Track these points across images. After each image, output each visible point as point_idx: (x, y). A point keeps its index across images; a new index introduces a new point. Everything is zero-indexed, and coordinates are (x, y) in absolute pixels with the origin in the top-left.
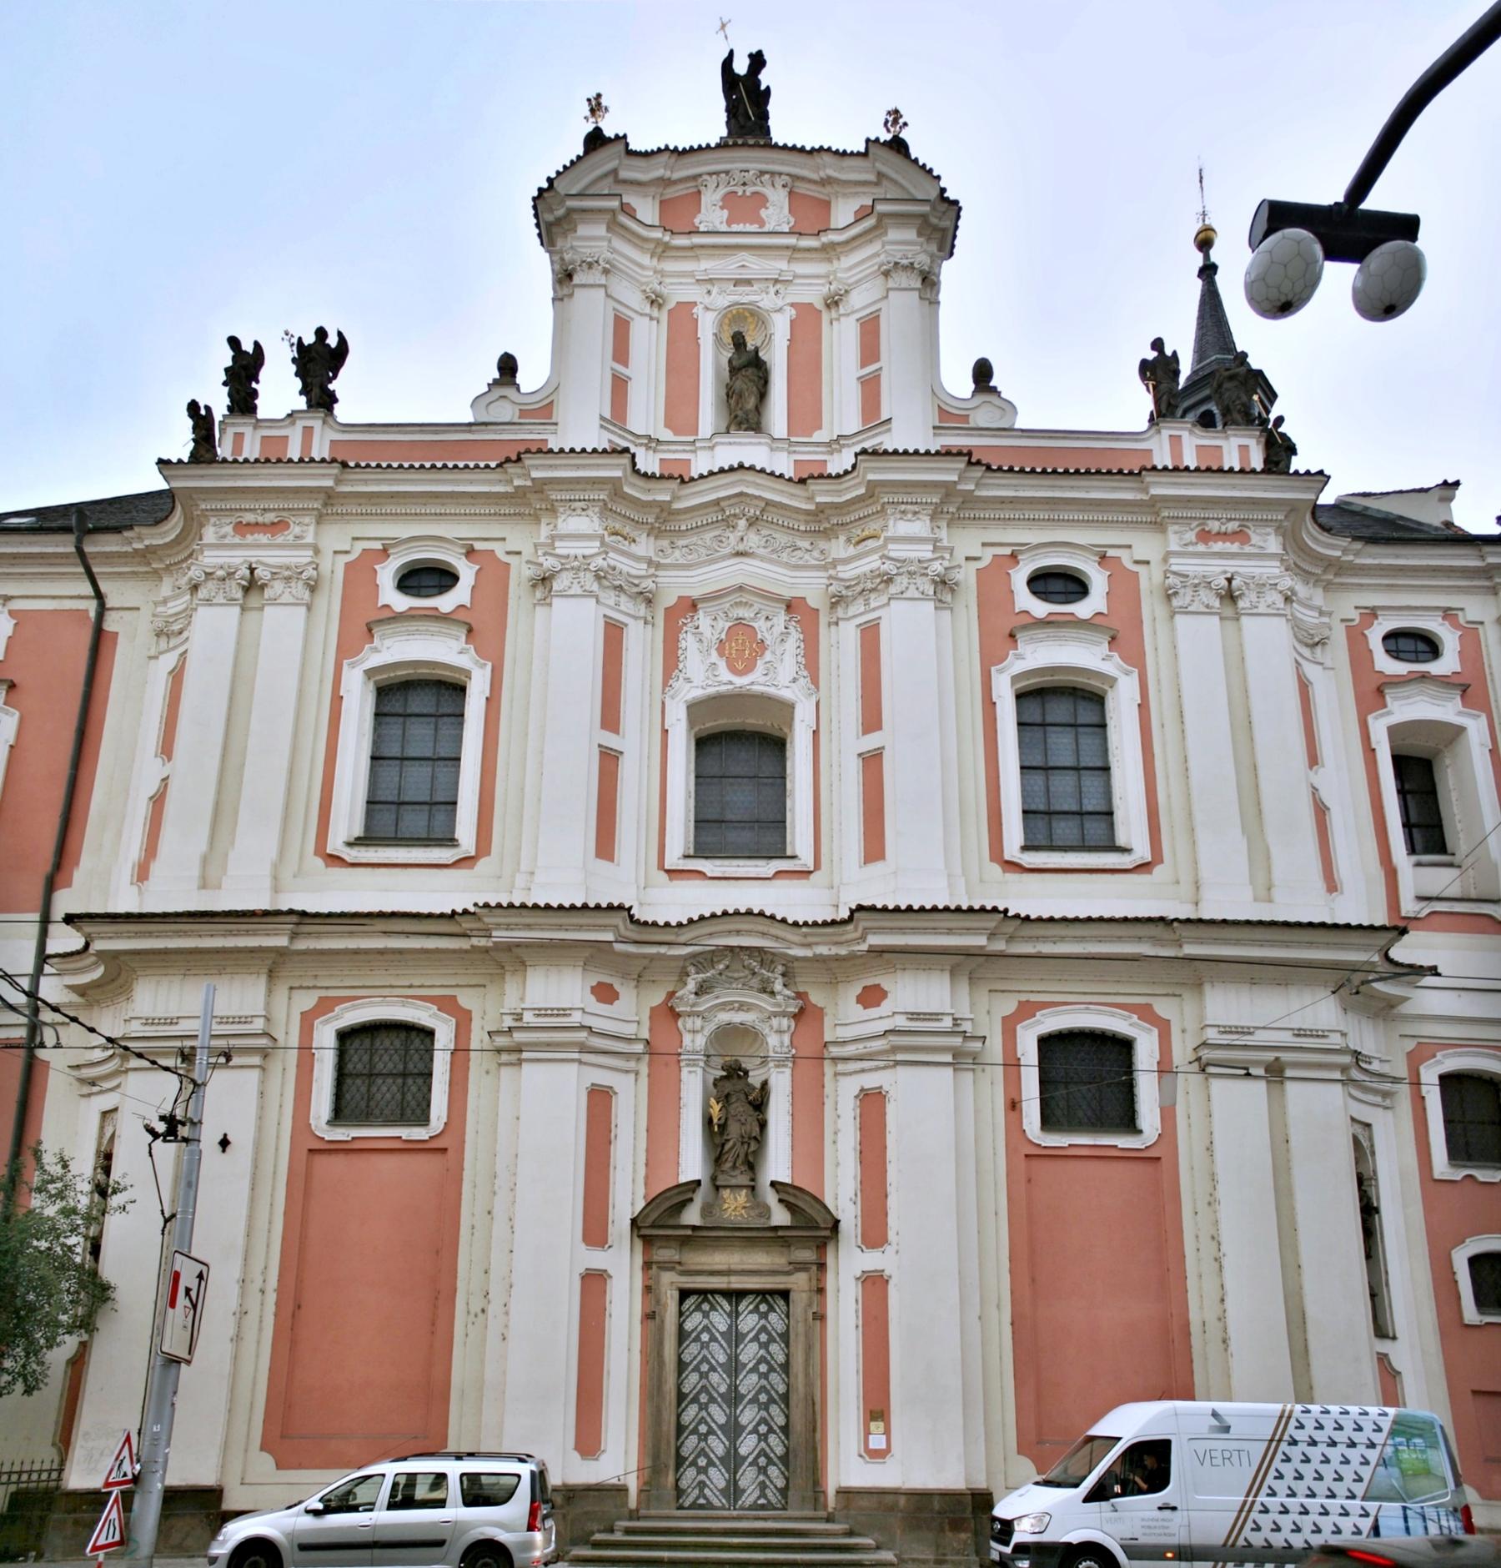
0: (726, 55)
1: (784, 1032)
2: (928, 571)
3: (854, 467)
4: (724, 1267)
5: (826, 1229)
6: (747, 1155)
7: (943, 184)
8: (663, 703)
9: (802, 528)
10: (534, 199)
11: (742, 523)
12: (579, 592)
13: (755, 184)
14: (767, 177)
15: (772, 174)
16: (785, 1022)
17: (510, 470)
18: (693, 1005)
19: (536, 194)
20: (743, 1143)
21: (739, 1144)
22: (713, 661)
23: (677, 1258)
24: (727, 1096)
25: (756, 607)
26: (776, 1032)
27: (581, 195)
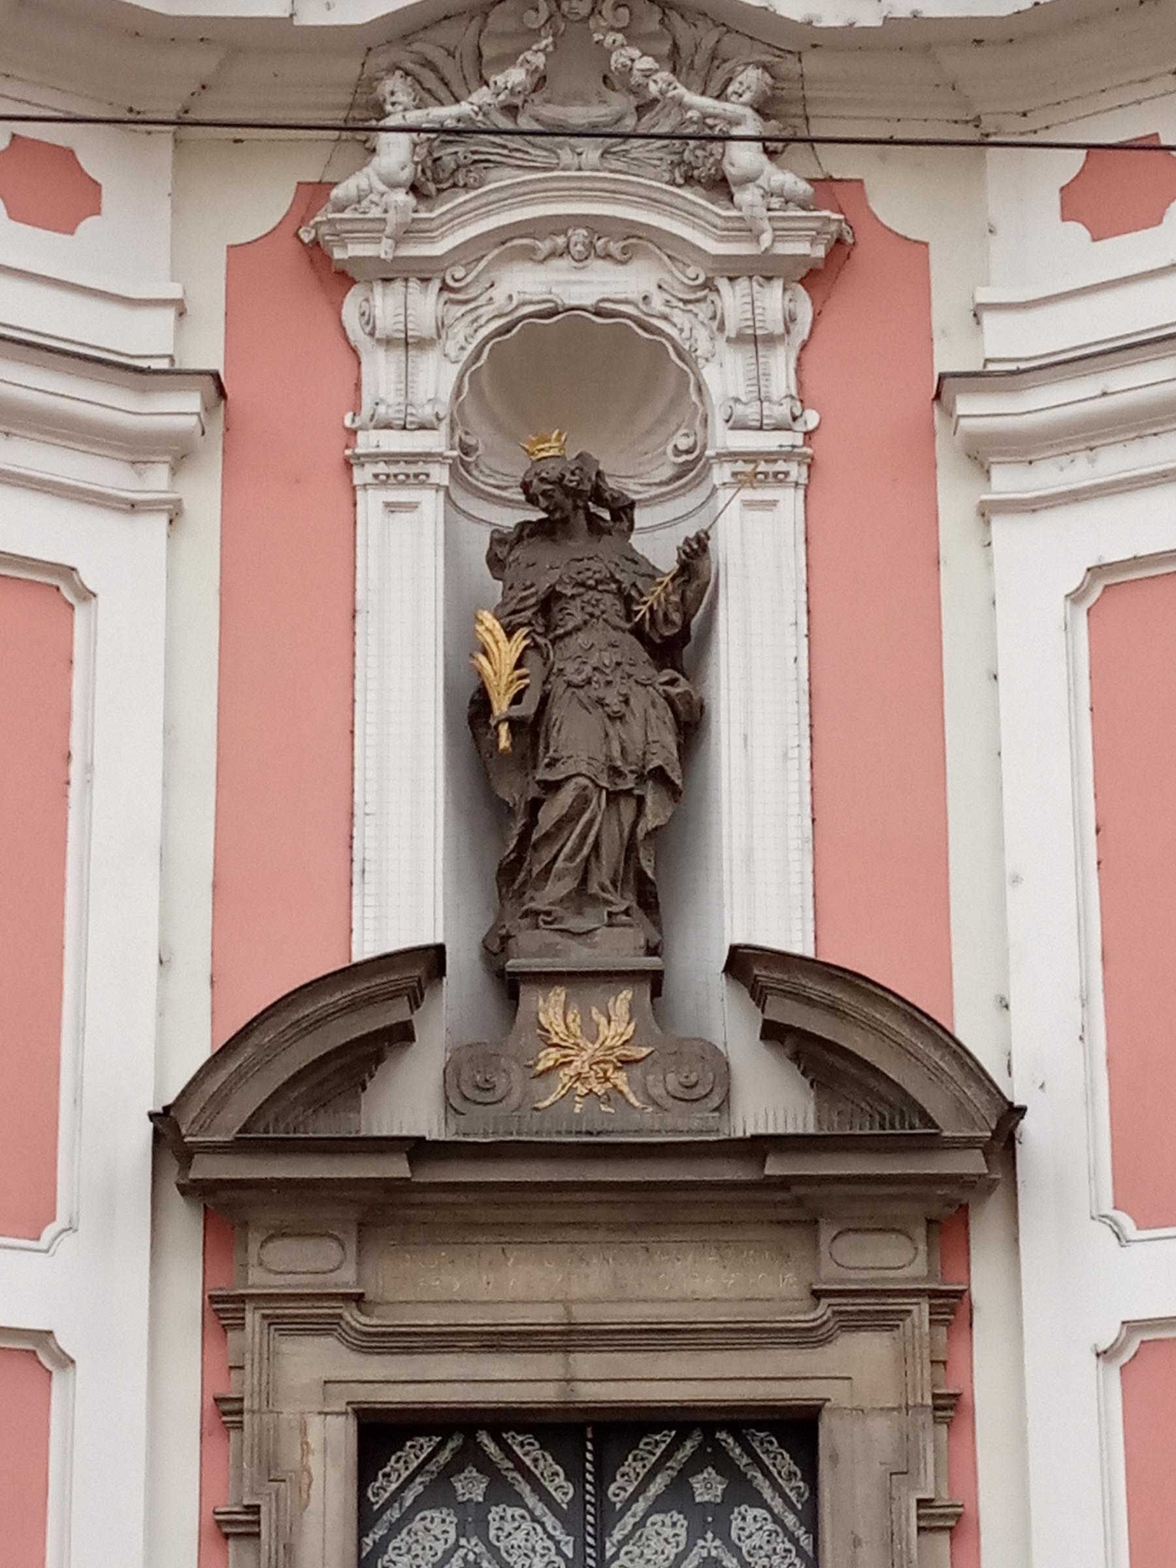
1: (771, 340)
5: (968, 1144)
6: (630, 849)
18: (408, 232)
20: (614, 797)
24: (549, 603)
26: (739, 339)
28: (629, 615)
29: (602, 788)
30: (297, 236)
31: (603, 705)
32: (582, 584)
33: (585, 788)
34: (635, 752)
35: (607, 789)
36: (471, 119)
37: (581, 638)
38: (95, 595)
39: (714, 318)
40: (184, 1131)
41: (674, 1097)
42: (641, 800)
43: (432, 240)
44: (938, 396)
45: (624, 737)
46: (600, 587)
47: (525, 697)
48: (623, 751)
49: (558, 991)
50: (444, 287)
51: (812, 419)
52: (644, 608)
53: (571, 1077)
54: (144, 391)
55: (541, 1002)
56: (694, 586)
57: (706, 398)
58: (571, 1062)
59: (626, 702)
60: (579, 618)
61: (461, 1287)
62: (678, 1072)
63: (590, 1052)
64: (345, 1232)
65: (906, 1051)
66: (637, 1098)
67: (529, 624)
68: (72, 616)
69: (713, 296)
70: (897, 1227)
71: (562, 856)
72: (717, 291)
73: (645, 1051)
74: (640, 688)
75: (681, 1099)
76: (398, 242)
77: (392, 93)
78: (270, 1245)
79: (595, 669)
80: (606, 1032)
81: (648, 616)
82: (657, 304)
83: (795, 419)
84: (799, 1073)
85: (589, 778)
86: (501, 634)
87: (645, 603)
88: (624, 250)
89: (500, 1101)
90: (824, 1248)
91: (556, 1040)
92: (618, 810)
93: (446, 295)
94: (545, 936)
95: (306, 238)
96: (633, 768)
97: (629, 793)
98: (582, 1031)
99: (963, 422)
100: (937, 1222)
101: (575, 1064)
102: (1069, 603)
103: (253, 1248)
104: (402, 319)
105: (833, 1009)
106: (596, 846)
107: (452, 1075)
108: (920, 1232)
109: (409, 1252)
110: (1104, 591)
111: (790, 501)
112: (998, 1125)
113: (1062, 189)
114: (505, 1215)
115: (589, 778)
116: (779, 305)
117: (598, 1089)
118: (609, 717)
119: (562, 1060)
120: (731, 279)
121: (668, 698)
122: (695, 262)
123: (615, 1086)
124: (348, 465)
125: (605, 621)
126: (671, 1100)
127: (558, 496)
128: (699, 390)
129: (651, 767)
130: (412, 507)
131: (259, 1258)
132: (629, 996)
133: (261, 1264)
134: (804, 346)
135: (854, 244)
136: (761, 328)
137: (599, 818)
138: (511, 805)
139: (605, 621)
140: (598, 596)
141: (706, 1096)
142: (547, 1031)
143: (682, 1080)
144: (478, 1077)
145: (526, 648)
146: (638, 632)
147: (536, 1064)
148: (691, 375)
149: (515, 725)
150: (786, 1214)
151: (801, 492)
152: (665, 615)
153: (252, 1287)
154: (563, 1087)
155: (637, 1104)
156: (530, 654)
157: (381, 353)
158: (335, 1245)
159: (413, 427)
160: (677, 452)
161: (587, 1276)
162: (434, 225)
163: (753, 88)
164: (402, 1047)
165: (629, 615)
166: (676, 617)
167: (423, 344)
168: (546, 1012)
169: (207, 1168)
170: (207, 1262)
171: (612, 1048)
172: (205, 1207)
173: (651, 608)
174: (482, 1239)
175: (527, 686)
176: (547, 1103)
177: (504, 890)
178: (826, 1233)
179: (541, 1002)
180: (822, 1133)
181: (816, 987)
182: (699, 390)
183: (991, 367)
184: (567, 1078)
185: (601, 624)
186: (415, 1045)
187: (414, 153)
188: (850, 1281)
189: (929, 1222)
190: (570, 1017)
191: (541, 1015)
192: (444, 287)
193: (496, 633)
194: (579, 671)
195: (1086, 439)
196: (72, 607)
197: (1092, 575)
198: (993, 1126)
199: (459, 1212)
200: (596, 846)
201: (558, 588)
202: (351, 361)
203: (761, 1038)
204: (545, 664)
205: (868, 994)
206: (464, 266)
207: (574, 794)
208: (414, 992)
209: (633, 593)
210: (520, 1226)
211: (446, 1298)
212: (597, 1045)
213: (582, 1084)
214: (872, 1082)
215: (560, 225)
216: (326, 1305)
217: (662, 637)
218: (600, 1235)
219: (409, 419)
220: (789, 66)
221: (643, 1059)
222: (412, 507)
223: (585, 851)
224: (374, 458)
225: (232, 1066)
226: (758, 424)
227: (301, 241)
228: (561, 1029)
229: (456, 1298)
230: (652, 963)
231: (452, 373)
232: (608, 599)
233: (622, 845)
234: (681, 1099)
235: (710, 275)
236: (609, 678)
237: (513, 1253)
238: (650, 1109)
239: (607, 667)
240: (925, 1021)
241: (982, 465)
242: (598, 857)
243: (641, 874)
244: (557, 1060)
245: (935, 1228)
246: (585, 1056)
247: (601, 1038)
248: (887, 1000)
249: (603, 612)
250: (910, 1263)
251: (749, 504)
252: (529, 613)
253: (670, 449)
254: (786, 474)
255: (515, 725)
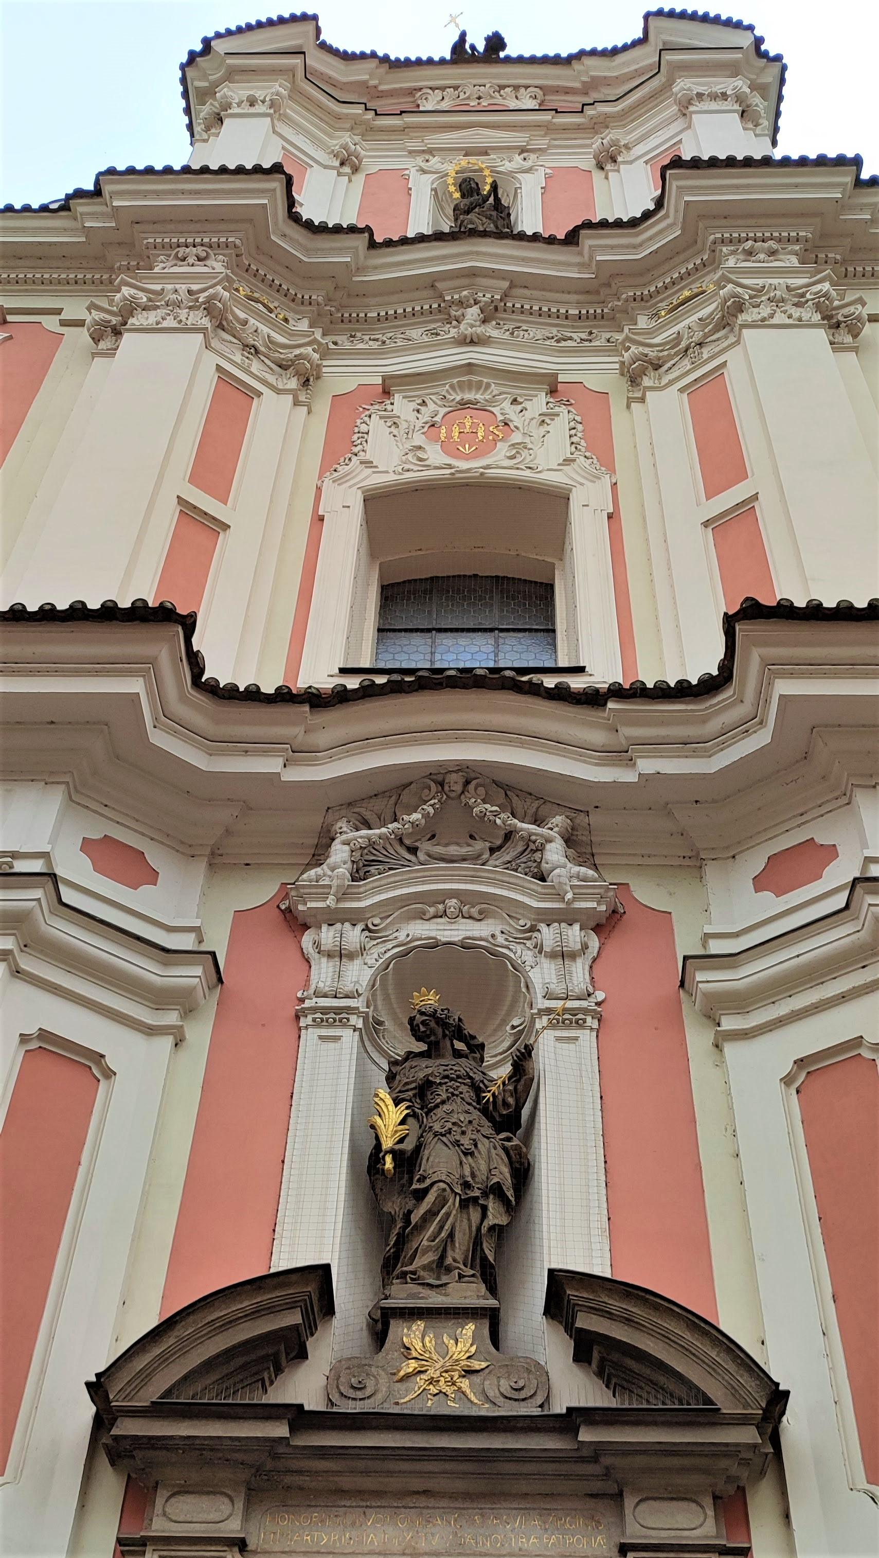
0: (456, 38)
1: (573, 956)
2: (808, 296)
3: (660, 203)
4: (478, 936)
5: (742, 1421)
6: (477, 1242)
7: (758, 33)
8: (319, 489)
9: (573, 312)
10: (183, 67)
11: (473, 313)
12: (175, 324)
13: (492, 97)
14: (508, 90)
15: (516, 88)
16: (574, 935)
17: (80, 209)
18: (344, 895)
19: (184, 58)
20: (465, 1204)
21: (453, 1204)
22: (417, 443)
23: (233, 1527)
24: (425, 1088)
25: (494, 389)
26: (553, 955)
27: (158, 1410)
28: (479, 1099)
29: (456, 1194)
30: (278, 906)
31: (458, 1146)
32: (447, 1077)
33: (444, 1190)
34: (482, 1176)
35: (460, 1195)
36: (387, 837)
37: (446, 1107)
38: (115, 1074)
39: (535, 947)
40: (111, 1397)
41: (506, 1397)
42: (484, 1209)
43: (359, 899)
44: (682, 984)
45: (473, 1165)
46: (460, 1080)
47: (406, 1141)
48: (473, 1175)
49: (419, 1323)
50: (367, 928)
51: (600, 996)
52: (489, 1095)
53: (426, 1381)
54: (166, 964)
55: (405, 1330)
56: (522, 1082)
57: (532, 990)
58: (426, 1371)
59: (476, 1146)
60: (444, 1096)
61: (329, 1540)
62: (508, 1378)
63: (441, 1364)
64: (235, 1491)
65: (686, 1351)
66: (476, 1397)
67: (410, 1101)
68: (98, 1085)
69: (535, 934)
70: (688, 1496)
71: (425, 1238)
72: (539, 930)
73: (484, 1365)
74: (485, 1139)
75: (510, 1399)
76: (338, 900)
77: (341, 828)
78: (173, 1500)
79: (454, 1124)
80: (454, 1349)
81: (491, 1099)
82: (501, 939)
83: (589, 995)
84: (604, 1386)
85: (448, 1184)
86: (390, 1102)
87: (489, 1091)
88: (480, 913)
89: (369, 1397)
90: (628, 1511)
91: (414, 1354)
92: (468, 1214)
93: (366, 933)
94: (412, 1288)
95: (283, 907)
96: (479, 1186)
97: (475, 1199)
98: (435, 1349)
99: (700, 985)
100: (721, 1498)
101: (428, 1372)
102: (783, 1085)
103: (159, 1501)
104: (339, 939)
105: (628, 1321)
106: (451, 1235)
107: (334, 1377)
108: (708, 1502)
109: (287, 1512)
110: (806, 1076)
111: (587, 1038)
112: (768, 1404)
113: (753, 879)
114: (369, 1483)
115: (448, 1184)
116: (578, 939)
117: (449, 1390)
118: (463, 1152)
119: (419, 1369)
120: (548, 925)
121: (505, 1149)
122: (523, 915)
123: (460, 1388)
124: (297, 1018)
125: (462, 1098)
126: (502, 1399)
127: (433, 1024)
128: (527, 987)
129: (492, 1183)
130: (337, 1039)
131: (163, 1510)
132: (473, 1327)
133: (164, 1514)
134: (594, 960)
135: (625, 912)
136: (565, 946)
137: (454, 1212)
138: (393, 1213)
139: (462, 1098)
140: (459, 1084)
141: (531, 1397)
142: (409, 1349)
143: (513, 1384)
144: (353, 1380)
145: (407, 1115)
146: (485, 1111)
147: (399, 1371)
148: (522, 978)
149: (397, 1155)
150: (597, 1486)
151: (594, 1034)
152: (504, 1100)
153: (153, 1531)
154: (419, 1388)
155: (476, 1401)
156: (411, 1120)
157: (324, 960)
158: (226, 1500)
159: (341, 996)
160: (513, 1027)
161: (433, 1535)
162: (362, 890)
163: (560, 825)
164: (299, 1363)
165: (479, 1099)
166: (511, 1100)
167: (351, 956)
168: (408, 1336)
169: (128, 1427)
170: (123, 1520)
171: (457, 1360)
172: (129, 1476)
173: (494, 1094)
174: (348, 1503)
175: (408, 1134)
176: (405, 1400)
177: (386, 1280)
178: (629, 1502)
179: (405, 1330)
180: (624, 1407)
181: (615, 1304)
182: (527, 987)
183: (715, 947)
184: (423, 1381)
185: (459, 1100)
186: (307, 1362)
187: (352, 856)
188: (653, 1538)
189: (715, 1498)
190: (427, 1339)
191: (405, 1339)
192: (367, 928)
193: (386, 1100)
194: (443, 1127)
195: (787, 990)
196: (99, 1081)
197: (798, 1066)
198: (764, 1406)
199: (331, 1479)
200: (451, 1235)
201: (430, 1078)
202: (306, 963)
203: (574, 1360)
204: (420, 1127)
205: (656, 1308)
206: (381, 918)
207: (435, 1195)
208: (306, 1305)
209: (481, 1085)
210: (378, 1494)
211: (315, 1550)
212: (447, 1358)
213: (434, 1386)
214: (662, 1380)
215: (441, 897)
216: (213, 1548)
217: (501, 1115)
218: (444, 1503)
219: (338, 990)
220: (582, 819)
221: (482, 1369)
222: (337, 1039)
223: (443, 1234)
224: (314, 1010)
225: (157, 1351)
226: (565, 996)
227: (281, 910)
228: (419, 1346)
229: (323, 1550)
230: (492, 1302)
231: (368, 974)
232: (464, 1089)
233: (470, 1237)
234: (510, 1399)
235: (533, 923)
236: (464, 1129)
237: (373, 1515)
238: (487, 1406)
239: (462, 1122)
240: (703, 1325)
241: (714, 1020)
242: (453, 1241)
243: (484, 1259)
244: (416, 1368)
245: (720, 1501)
246: (438, 1366)
247: (450, 1354)
248: (672, 1309)
249: (461, 1093)
250: (701, 1525)
251: (558, 1039)
252: (411, 1093)
253: (508, 1028)
254: (585, 1022)
255: (397, 1155)
